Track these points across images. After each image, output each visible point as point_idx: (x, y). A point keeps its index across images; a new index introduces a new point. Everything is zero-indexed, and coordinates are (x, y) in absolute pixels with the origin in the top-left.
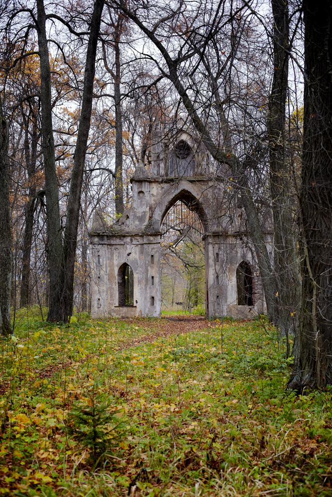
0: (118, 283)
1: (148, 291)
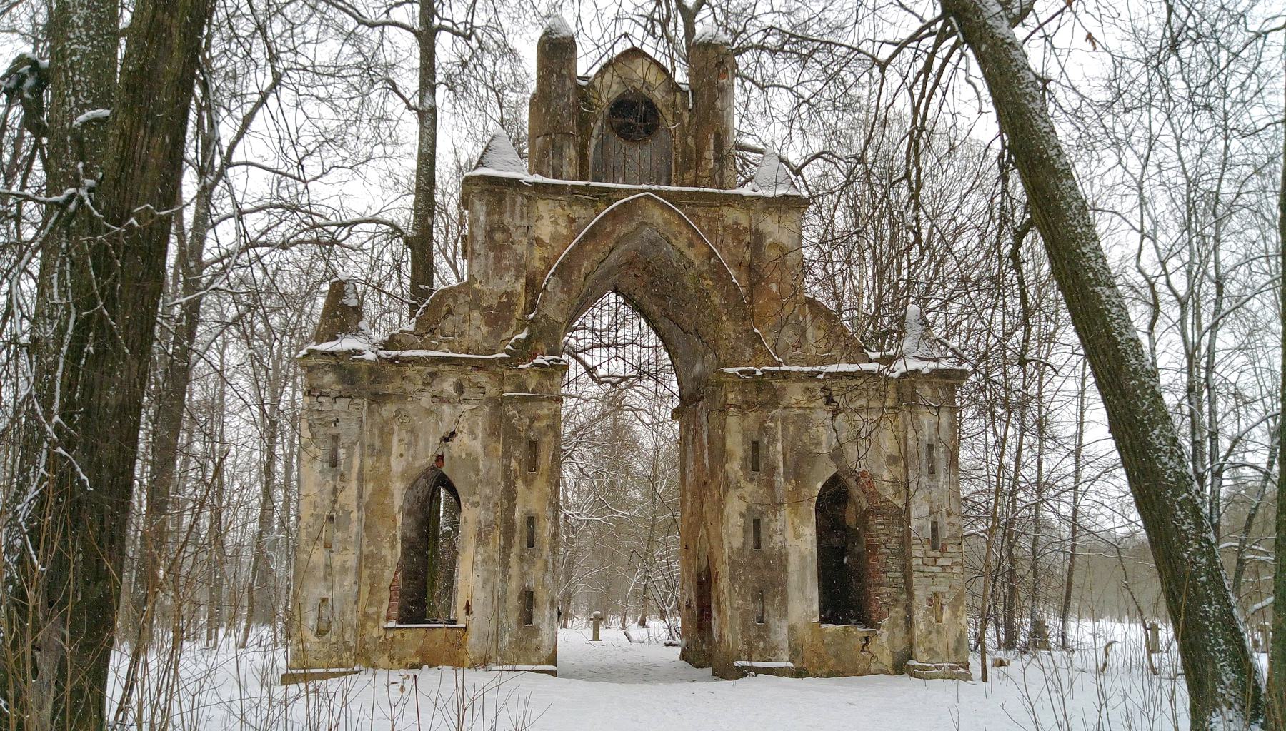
1: (514, 570)
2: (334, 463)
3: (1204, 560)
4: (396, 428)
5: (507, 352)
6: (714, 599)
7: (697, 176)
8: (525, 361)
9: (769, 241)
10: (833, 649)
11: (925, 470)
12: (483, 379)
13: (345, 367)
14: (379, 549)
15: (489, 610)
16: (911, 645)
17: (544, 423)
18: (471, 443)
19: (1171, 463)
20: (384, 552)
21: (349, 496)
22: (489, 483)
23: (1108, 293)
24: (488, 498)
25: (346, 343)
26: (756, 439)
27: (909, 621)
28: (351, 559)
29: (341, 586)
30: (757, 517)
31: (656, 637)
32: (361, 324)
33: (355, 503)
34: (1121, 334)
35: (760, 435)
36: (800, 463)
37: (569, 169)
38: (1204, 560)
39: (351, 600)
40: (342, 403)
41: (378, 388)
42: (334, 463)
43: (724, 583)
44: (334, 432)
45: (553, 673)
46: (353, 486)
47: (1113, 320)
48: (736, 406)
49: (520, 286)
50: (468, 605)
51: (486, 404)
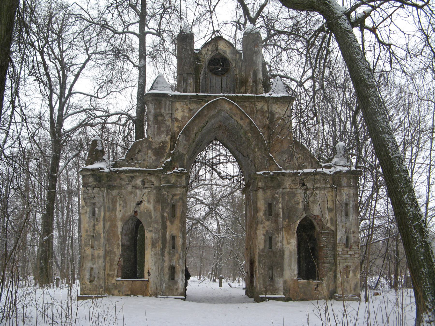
0: (123, 245)
1: (167, 258)
2: (93, 214)
3: (423, 250)
4: (118, 200)
5: (162, 167)
6: (254, 270)
7: (246, 89)
8: (170, 171)
9: (277, 116)
10: (302, 290)
11: (343, 213)
12: (153, 179)
13: (97, 174)
14: (113, 249)
15: (157, 274)
16: (336, 287)
17: (178, 197)
18: (148, 205)
19: (411, 209)
20: (115, 250)
21: (100, 227)
22: (156, 222)
23: (388, 137)
24: (156, 229)
25: (96, 165)
26: (270, 202)
27: (335, 277)
28: (101, 252)
29: (98, 263)
30: (270, 235)
31: (239, 286)
32: (104, 157)
33: (102, 230)
34: (393, 155)
35: (272, 200)
36: (290, 213)
37: (190, 88)
38: (423, 250)
39: (102, 268)
40: (96, 190)
41: (110, 183)
42: (93, 214)
43: (257, 264)
44: (93, 201)
45: (184, 299)
46: (102, 223)
47: (389, 148)
48: (261, 188)
49: (168, 139)
50: (149, 271)
51: (154, 189)
